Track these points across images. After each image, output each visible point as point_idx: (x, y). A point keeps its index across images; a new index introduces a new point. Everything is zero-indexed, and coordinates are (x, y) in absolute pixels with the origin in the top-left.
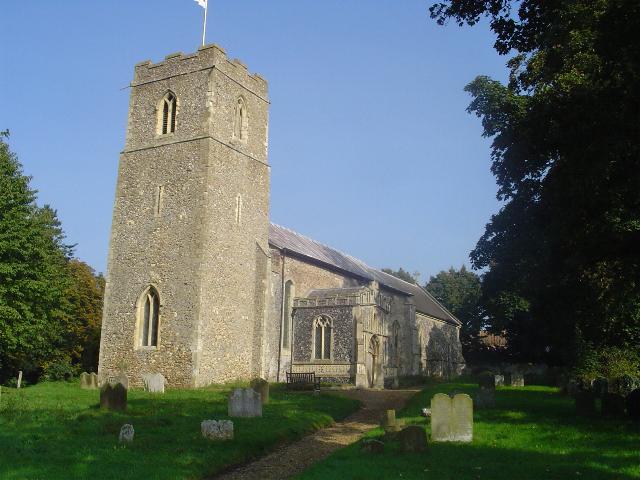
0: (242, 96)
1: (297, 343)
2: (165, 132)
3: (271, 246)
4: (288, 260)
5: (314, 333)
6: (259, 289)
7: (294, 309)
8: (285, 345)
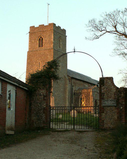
0: (60, 36)
1: (75, 102)
2: (40, 46)
3: (68, 76)
4: (73, 80)
5: (80, 99)
6: (65, 89)
7: (74, 93)
8: (72, 103)
